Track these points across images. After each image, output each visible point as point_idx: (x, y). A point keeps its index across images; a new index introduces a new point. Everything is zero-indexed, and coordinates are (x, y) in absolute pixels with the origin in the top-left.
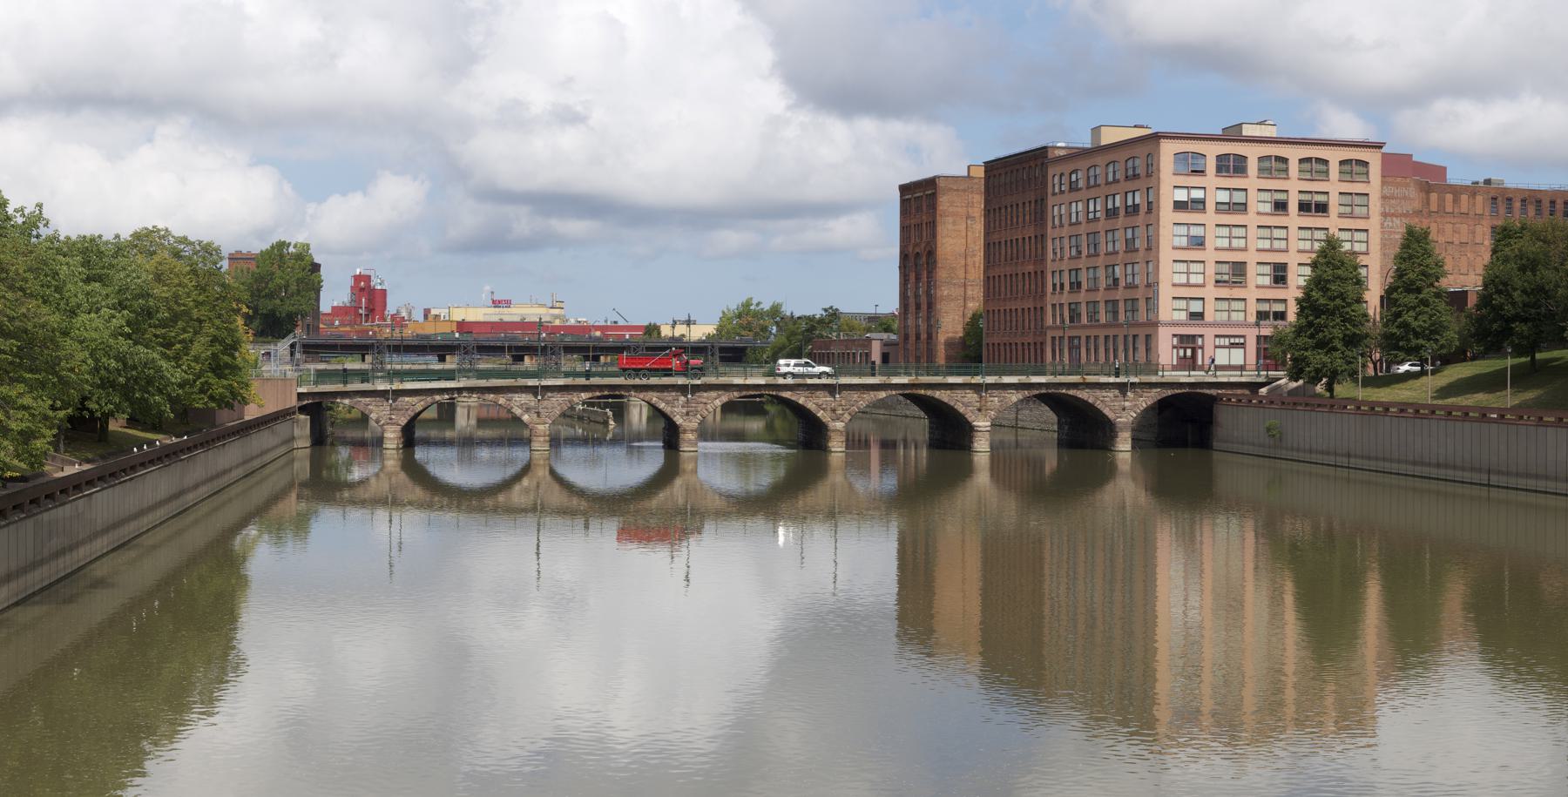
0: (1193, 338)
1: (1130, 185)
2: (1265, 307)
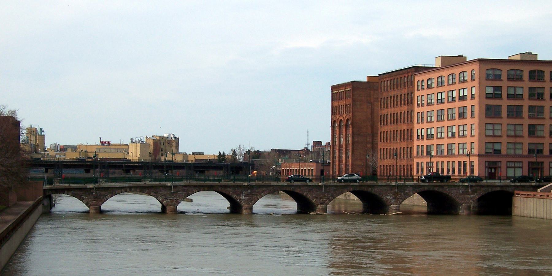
0: (495, 163)
1: (462, 86)
2: (533, 147)
